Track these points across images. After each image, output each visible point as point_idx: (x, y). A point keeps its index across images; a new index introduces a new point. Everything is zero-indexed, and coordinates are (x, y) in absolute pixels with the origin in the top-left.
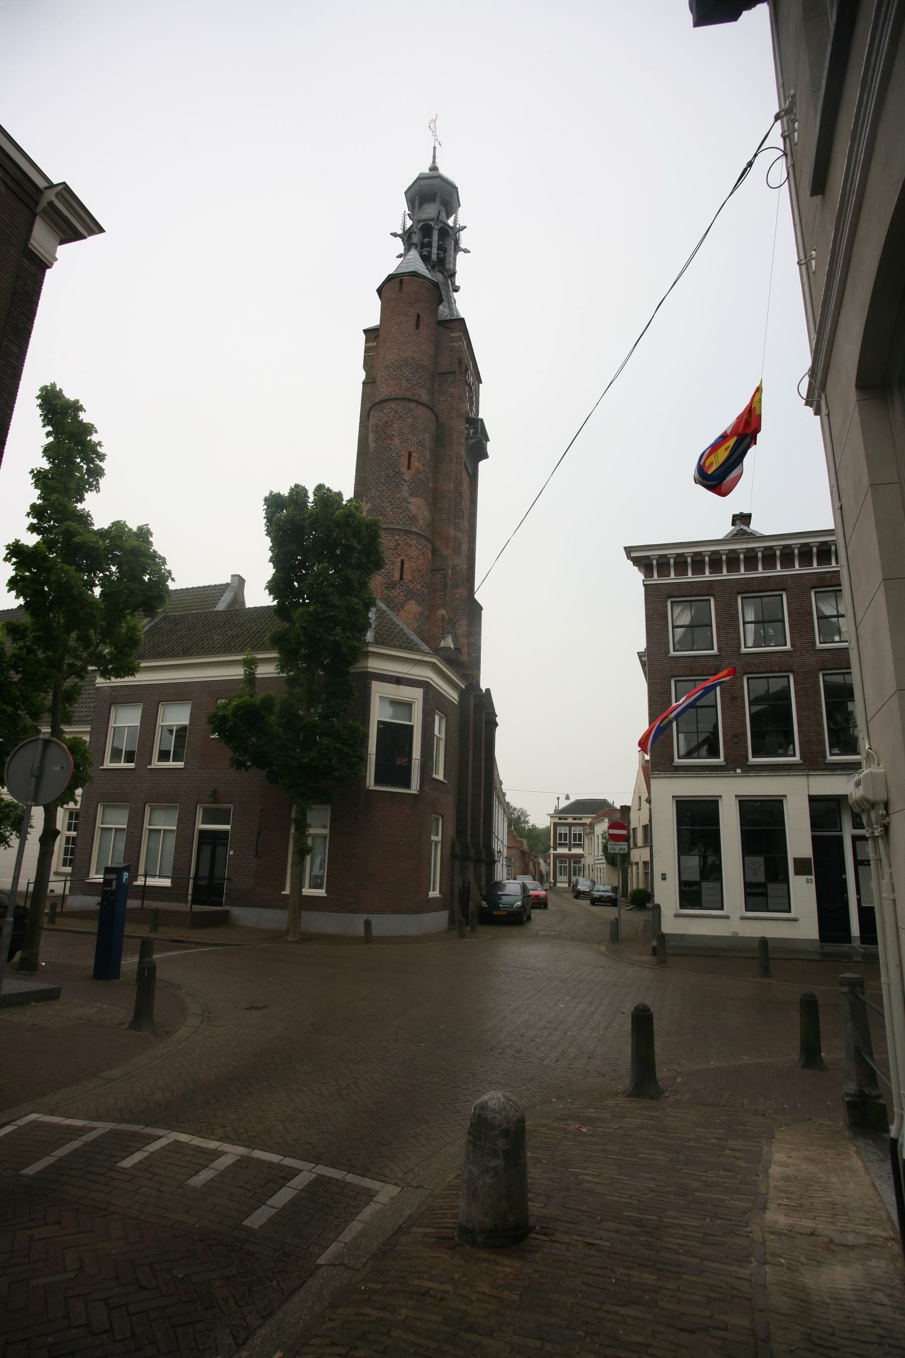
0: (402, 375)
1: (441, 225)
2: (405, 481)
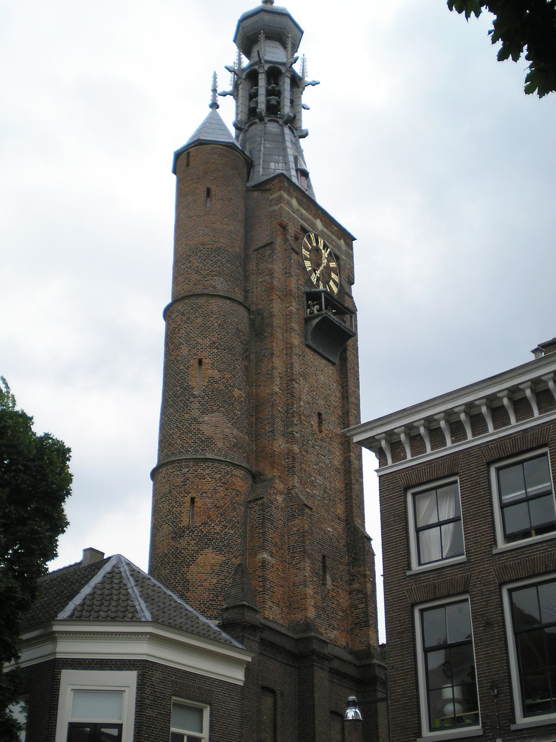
0: (190, 267)
1: (267, 66)
2: (196, 397)
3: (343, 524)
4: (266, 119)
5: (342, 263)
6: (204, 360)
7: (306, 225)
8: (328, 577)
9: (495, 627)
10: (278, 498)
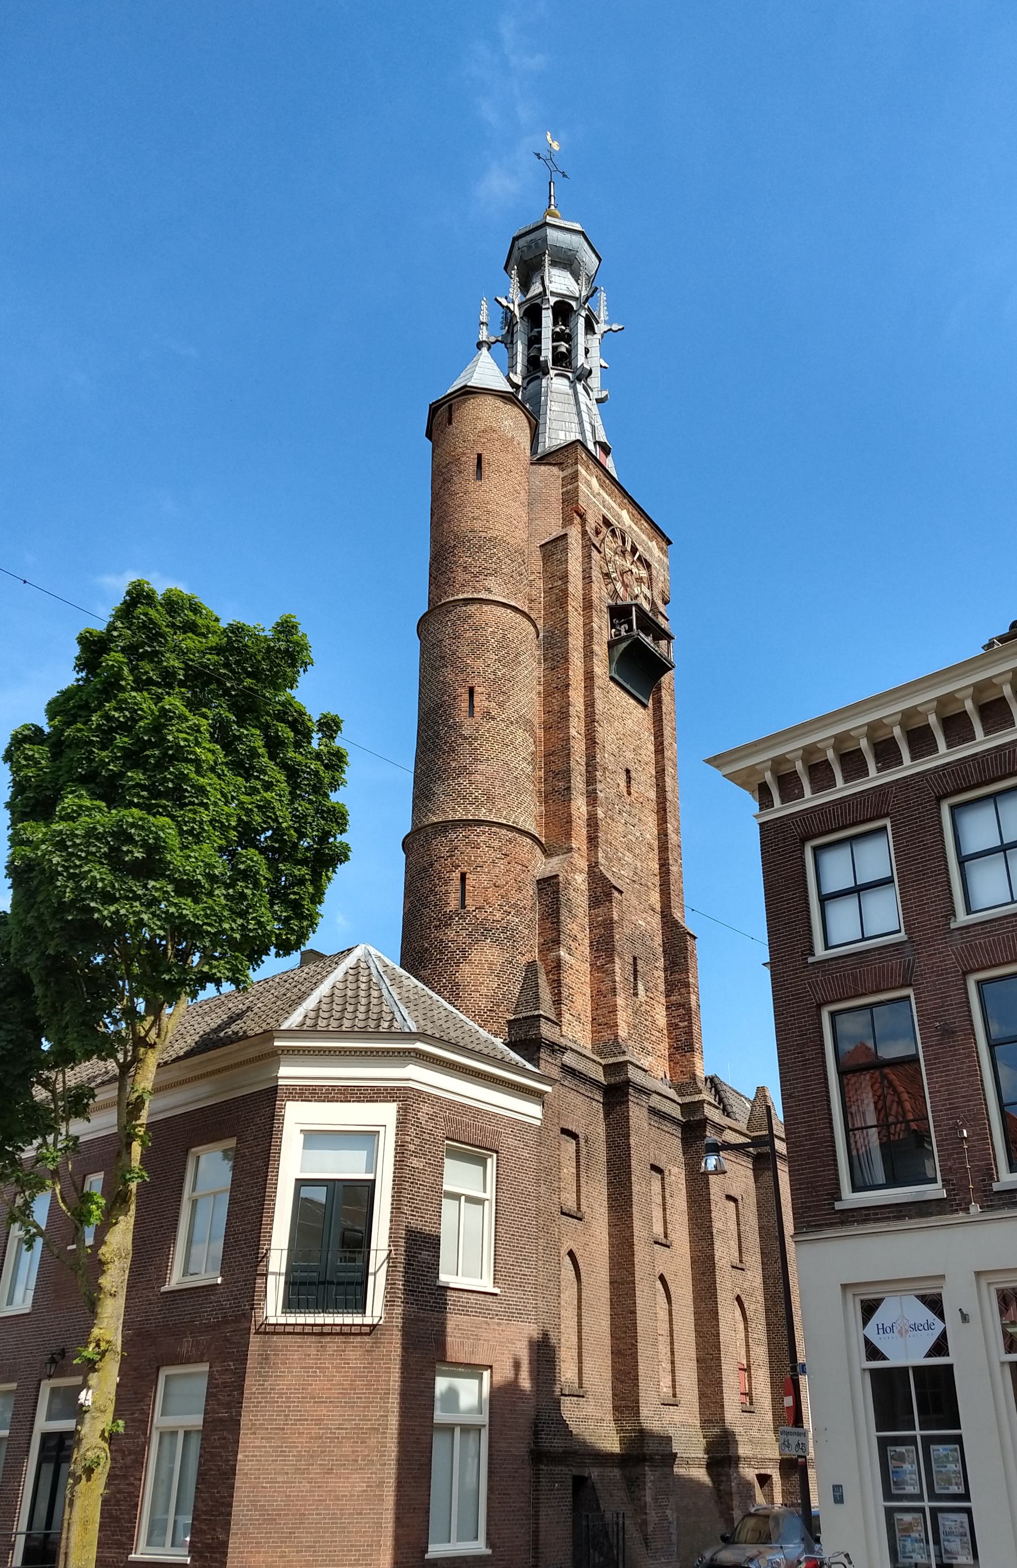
1: (553, 300)
3: (658, 918)
4: (552, 373)
5: (654, 572)
6: (477, 689)
7: (609, 517)
8: (641, 987)
9: (959, 1036)
10: (576, 877)
